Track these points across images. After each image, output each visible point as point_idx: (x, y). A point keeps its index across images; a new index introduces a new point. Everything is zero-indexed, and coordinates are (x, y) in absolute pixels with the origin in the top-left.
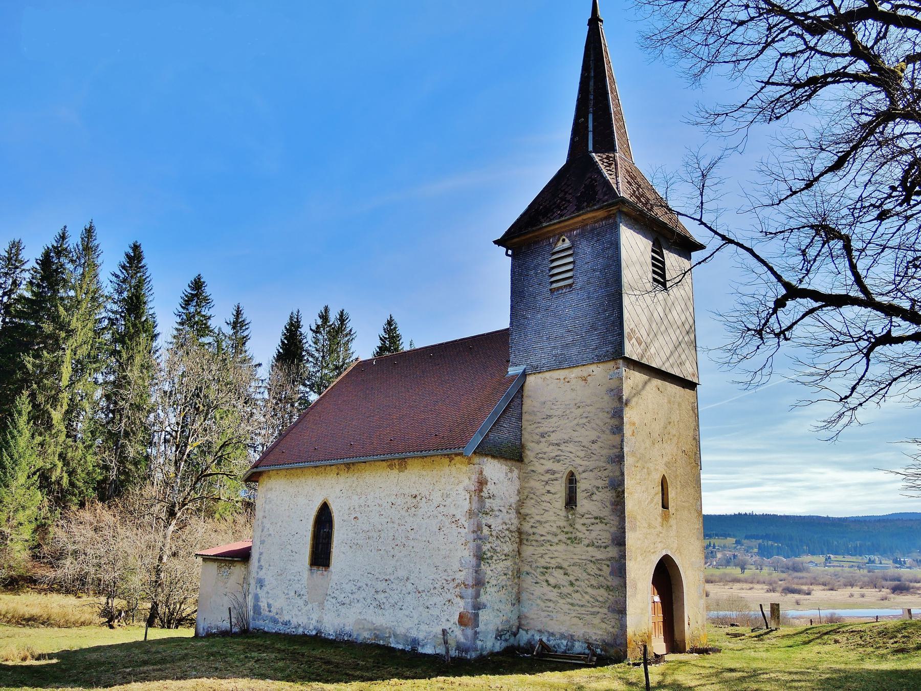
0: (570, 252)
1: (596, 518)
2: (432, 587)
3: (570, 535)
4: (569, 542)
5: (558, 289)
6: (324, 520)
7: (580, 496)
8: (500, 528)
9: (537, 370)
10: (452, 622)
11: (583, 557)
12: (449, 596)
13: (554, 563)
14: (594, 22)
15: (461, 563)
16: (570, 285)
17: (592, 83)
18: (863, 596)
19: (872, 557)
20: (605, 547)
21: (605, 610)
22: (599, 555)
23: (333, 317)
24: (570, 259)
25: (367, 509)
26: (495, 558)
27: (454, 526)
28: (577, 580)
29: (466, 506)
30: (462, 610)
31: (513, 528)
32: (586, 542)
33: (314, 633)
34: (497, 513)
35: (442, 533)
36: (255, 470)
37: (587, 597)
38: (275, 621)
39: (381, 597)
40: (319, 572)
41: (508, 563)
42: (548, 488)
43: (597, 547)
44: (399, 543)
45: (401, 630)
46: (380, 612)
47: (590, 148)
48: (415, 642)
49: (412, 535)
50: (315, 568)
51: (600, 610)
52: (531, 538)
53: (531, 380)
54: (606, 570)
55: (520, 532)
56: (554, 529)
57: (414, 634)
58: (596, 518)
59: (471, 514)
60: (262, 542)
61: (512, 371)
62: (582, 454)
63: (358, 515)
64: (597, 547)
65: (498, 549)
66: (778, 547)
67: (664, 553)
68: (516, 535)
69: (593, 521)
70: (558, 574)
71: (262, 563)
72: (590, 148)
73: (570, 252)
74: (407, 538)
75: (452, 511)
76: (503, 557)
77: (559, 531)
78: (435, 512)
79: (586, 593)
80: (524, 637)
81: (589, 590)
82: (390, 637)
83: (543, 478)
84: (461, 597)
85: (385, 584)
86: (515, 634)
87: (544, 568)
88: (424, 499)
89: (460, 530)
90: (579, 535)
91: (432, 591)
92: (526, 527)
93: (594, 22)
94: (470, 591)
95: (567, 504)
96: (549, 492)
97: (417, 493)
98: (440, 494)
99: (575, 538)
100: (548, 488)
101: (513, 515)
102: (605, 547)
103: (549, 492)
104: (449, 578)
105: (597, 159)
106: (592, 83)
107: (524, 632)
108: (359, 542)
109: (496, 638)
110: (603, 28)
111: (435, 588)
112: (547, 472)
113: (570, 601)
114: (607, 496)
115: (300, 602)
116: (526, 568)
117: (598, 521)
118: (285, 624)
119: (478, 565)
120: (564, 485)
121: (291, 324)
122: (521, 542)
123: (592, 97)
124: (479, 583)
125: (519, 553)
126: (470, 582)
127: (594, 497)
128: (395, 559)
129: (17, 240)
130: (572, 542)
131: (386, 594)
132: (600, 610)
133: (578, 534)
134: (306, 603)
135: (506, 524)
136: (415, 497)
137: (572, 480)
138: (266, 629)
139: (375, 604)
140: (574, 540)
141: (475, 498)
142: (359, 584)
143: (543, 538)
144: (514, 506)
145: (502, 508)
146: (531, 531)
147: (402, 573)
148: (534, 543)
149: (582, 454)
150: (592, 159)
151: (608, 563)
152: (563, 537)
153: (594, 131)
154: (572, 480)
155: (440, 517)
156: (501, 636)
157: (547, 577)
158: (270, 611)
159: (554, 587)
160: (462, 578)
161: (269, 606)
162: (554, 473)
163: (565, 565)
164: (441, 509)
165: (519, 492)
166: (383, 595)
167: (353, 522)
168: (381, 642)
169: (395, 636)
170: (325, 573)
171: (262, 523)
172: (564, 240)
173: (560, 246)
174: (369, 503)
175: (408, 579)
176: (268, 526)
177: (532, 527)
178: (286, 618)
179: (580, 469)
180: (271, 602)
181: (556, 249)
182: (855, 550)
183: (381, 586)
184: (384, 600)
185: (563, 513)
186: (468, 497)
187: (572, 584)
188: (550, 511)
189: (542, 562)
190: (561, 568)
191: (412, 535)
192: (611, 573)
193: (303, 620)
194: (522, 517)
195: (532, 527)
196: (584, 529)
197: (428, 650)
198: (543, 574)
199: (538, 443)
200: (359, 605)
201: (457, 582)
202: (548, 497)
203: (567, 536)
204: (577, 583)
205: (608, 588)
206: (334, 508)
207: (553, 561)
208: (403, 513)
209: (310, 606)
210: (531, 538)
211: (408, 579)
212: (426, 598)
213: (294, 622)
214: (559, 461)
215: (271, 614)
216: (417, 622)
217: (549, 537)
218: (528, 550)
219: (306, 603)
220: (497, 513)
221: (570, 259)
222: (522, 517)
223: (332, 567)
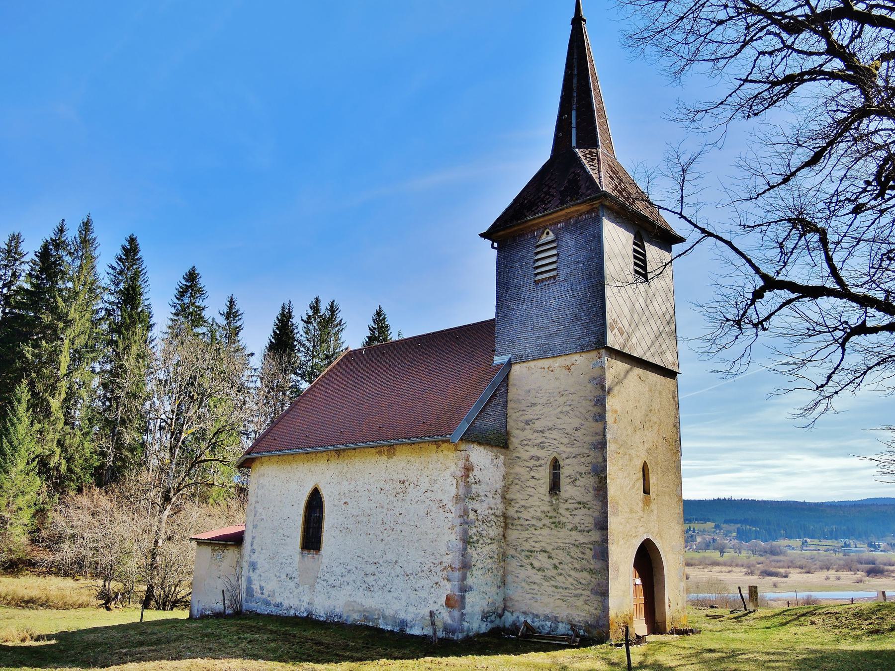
0: (554, 245)
1: (579, 503)
2: (420, 570)
3: (554, 520)
4: (553, 526)
6: (315, 505)
7: (564, 481)
8: (486, 513)
9: (522, 359)
10: (439, 604)
11: (567, 541)
12: (436, 579)
13: (538, 547)
14: (577, 21)
15: (448, 547)
16: (554, 277)
17: (575, 81)
18: (838, 579)
19: (848, 541)
20: (588, 532)
21: (588, 593)
22: (582, 539)
23: (324, 308)
24: (554, 252)
25: (357, 494)
26: (481, 541)
27: (441, 510)
28: (560, 563)
29: (453, 491)
30: (449, 592)
31: (499, 513)
32: (570, 526)
33: (305, 614)
34: (483, 498)
35: (429, 518)
36: (248, 456)
37: (571, 580)
38: (268, 603)
39: (370, 579)
40: (310, 556)
41: (494, 547)
42: (532, 474)
43: (580, 531)
44: (388, 527)
45: (389, 612)
46: (369, 594)
47: (574, 144)
48: (403, 623)
49: (400, 519)
51: (583, 592)
52: (516, 522)
54: (589, 554)
55: (505, 517)
56: (539, 514)
57: (402, 615)
58: (579, 503)
59: (458, 499)
60: (255, 526)
61: (498, 360)
62: (565, 441)
63: (348, 500)
64: (580, 531)
65: (484, 533)
66: (756, 532)
67: (645, 537)
68: (501, 519)
69: (576, 505)
70: (543, 557)
71: (255, 547)
72: (574, 144)
73: (554, 245)
75: (440, 496)
76: (489, 541)
77: (543, 516)
78: (423, 498)
79: (570, 576)
80: (509, 619)
81: (573, 573)
82: (379, 618)
84: (448, 580)
85: (374, 567)
86: (500, 616)
87: (528, 551)
89: (447, 515)
90: (563, 519)
91: (420, 574)
92: (511, 512)
93: (577, 21)
94: (457, 574)
95: (551, 490)
96: (533, 478)
97: (406, 479)
98: (427, 479)
99: (559, 523)
100: (532, 474)
101: (499, 500)
102: (588, 532)
103: (533, 478)
105: (580, 154)
106: (575, 81)
107: (509, 614)
109: (482, 619)
110: (586, 27)
111: (423, 571)
112: (532, 458)
113: (554, 583)
114: (590, 481)
115: (292, 585)
117: (581, 506)
118: (277, 606)
119: (465, 549)
121: (283, 315)
122: (506, 527)
123: (575, 95)
124: (466, 566)
125: (504, 537)
126: (457, 565)
127: (577, 483)
128: (384, 542)
130: (556, 526)
131: (375, 577)
132: (583, 592)
133: (562, 518)
134: (297, 586)
135: (492, 509)
136: (403, 483)
137: (555, 466)
138: (258, 611)
139: (364, 586)
140: (558, 525)
141: (462, 484)
142: (349, 567)
143: (527, 523)
144: (500, 491)
145: (488, 494)
146: (516, 516)
147: (390, 557)
148: (519, 527)
149: (565, 441)
150: (575, 154)
151: (591, 546)
152: (547, 521)
153: (577, 128)
154: (555, 466)
155: (428, 502)
156: (486, 618)
157: (532, 560)
158: (262, 594)
159: (539, 570)
160: (449, 561)
161: (262, 588)
162: (538, 459)
163: (549, 549)
164: (429, 494)
165: (504, 478)
166: (372, 578)
167: (343, 507)
169: (384, 617)
170: (316, 556)
172: (548, 233)
173: (545, 238)
174: (358, 488)
175: (396, 562)
176: (260, 510)
177: (517, 511)
179: (564, 456)
180: (263, 584)
181: (541, 242)
182: (831, 534)
183: (370, 569)
184: (374, 583)
185: (547, 498)
186: (454, 482)
187: (555, 567)
188: (534, 497)
189: (527, 546)
190: (545, 552)
191: (400, 519)
192: (594, 557)
193: (294, 602)
194: (507, 502)
195: (517, 511)
196: (567, 513)
197: (416, 631)
198: (528, 557)
199: (523, 430)
200: (349, 588)
201: (444, 565)
202: (532, 483)
203: (551, 520)
204: (561, 566)
205: (591, 571)
206: (325, 493)
207: (537, 545)
208: (392, 498)
209: (301, 588)
210: (516, 522)
211: (396, 562)
212: (414, 581)
213: (286, 603)
214: (543, 448)
215: (264, 596)
216: (405, 604)
217: (534, 522)
218: (513, 535)
219: (297, 586)
220: (483, 498)
221: (554, 252)
222: (507, 502)
223: (323, 551)
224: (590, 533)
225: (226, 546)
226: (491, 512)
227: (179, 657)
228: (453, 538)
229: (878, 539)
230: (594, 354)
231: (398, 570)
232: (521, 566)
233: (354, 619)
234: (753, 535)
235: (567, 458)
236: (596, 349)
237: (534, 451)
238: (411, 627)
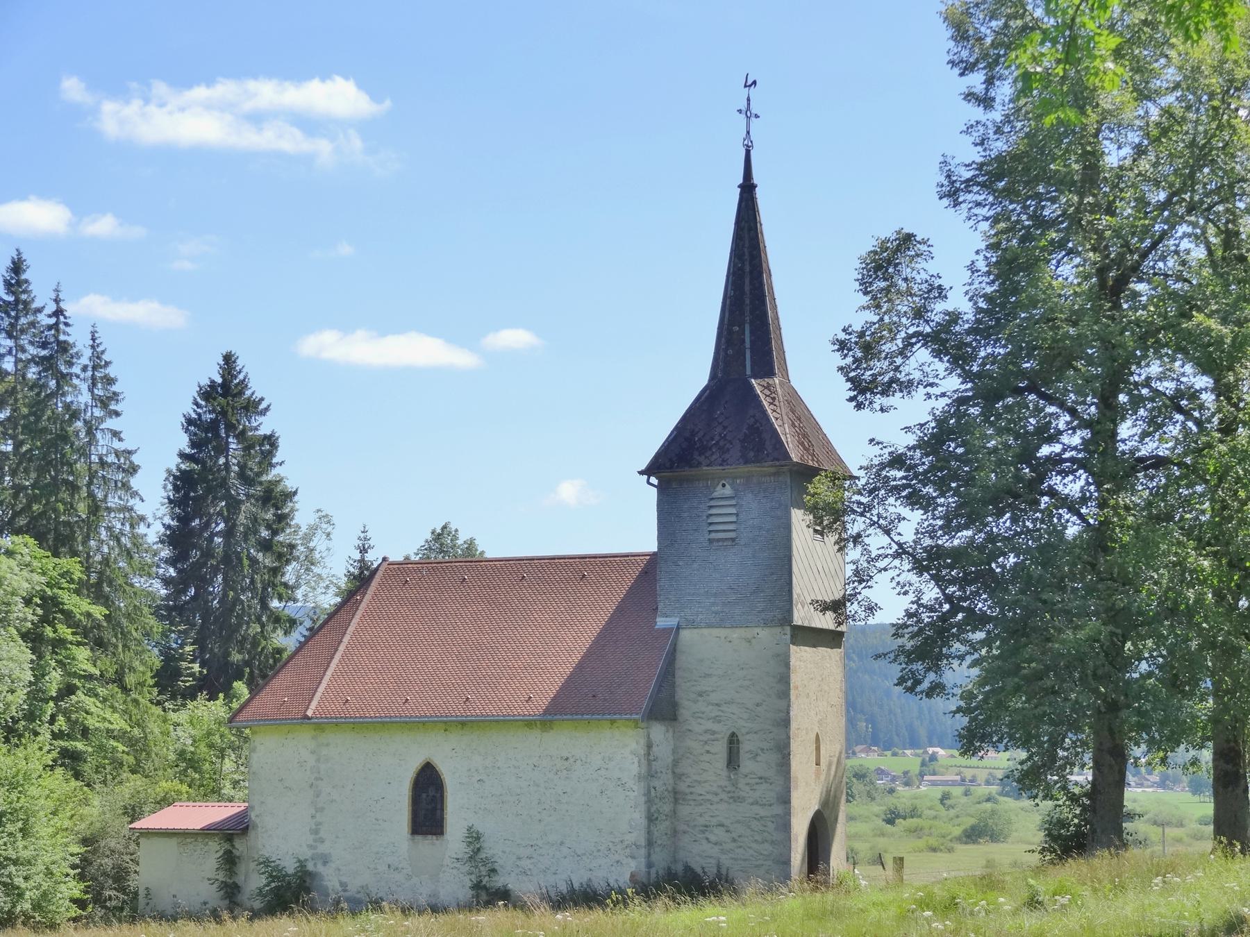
0: (733, 502)
5: (718, 540)
9: (692, 625)
12: (617, 857)
13: (714, 821)
14: (748, 189)
16: (733, 540)
17: (747, 281)
21: (769, 863)
22: (762, 812)
24: (733, 511)
27: (620, 789)
29: (635, 769)
32: (751, 800)
37: (751, 852)
39: (526, 863)
40: (426, 844)
41: (667, 823)
42: (707, 748)
46: (525, 878)
47: (748, 372)
52: (689, 797)
53: (685, 635)
54: (771, 826)
55: (675, 792)
56: (715, 789)
59: (640, 778)
61: (662, 622)
62: (745, 716)
63: (484, 777)
70: (720, 832)
72: (748, 372)
73: (733, 502)
77: (719, 791)
81: (754, 845)
83: (701, 738)
84: (633, 857)
92: (682, 787)
93: (748, 189)
94: (643, 851)
96: (708, 752)
100: (707, 748)
101: (670, 776)
103: (708, 752)
104: (617, 840)
105: (758, 390)
106: (747, 281)
110: (759, 193)
112: (706, 731)
114: (774, 757)
116: (683, 827)
119: (649, 827)
122: (676, 801)
123: (748, 301)
124: (650, 843)
126: (643, 842)
127: (759, 759)
137: (733, 742)
140: (737, 799)
141: (644, 762)
146: (688, 791)
149: (745, 716)
150: (752, 388)
152: (724, 796)
153: (752, 349)
154: (733, 742)
157: (707, 835)
158: (345, 891)
159: (716, 844)
162: (714, 733)
163: (727, 822)
164: (603, 772)
172: (724, 485)
173: (719, 491)
179: (744, 731)
180: (344, 879)
181: (716, 494)
185: (725, 773)
186: (636, 760)
187: (734, 840)
188: (709, 770)
189: (701, 821)
190: (723, 825)
194: (678, 776)
196: (747, 788)
198: (703, 832)
199: (695, 702)
202: (707, 757)
205: (773, 842)
210: (689, 797)
211: (562, 843)
214: (719, 722)
215: (347, 894)
217: (709, 797)
218: (684, 810)
219: (409, 877)
221: (733, 511)
222: (678, 776)
227: (836, 819)
228: (639, 817)
230: (778, 630)
236: (782, 625)
237: (710, 725)
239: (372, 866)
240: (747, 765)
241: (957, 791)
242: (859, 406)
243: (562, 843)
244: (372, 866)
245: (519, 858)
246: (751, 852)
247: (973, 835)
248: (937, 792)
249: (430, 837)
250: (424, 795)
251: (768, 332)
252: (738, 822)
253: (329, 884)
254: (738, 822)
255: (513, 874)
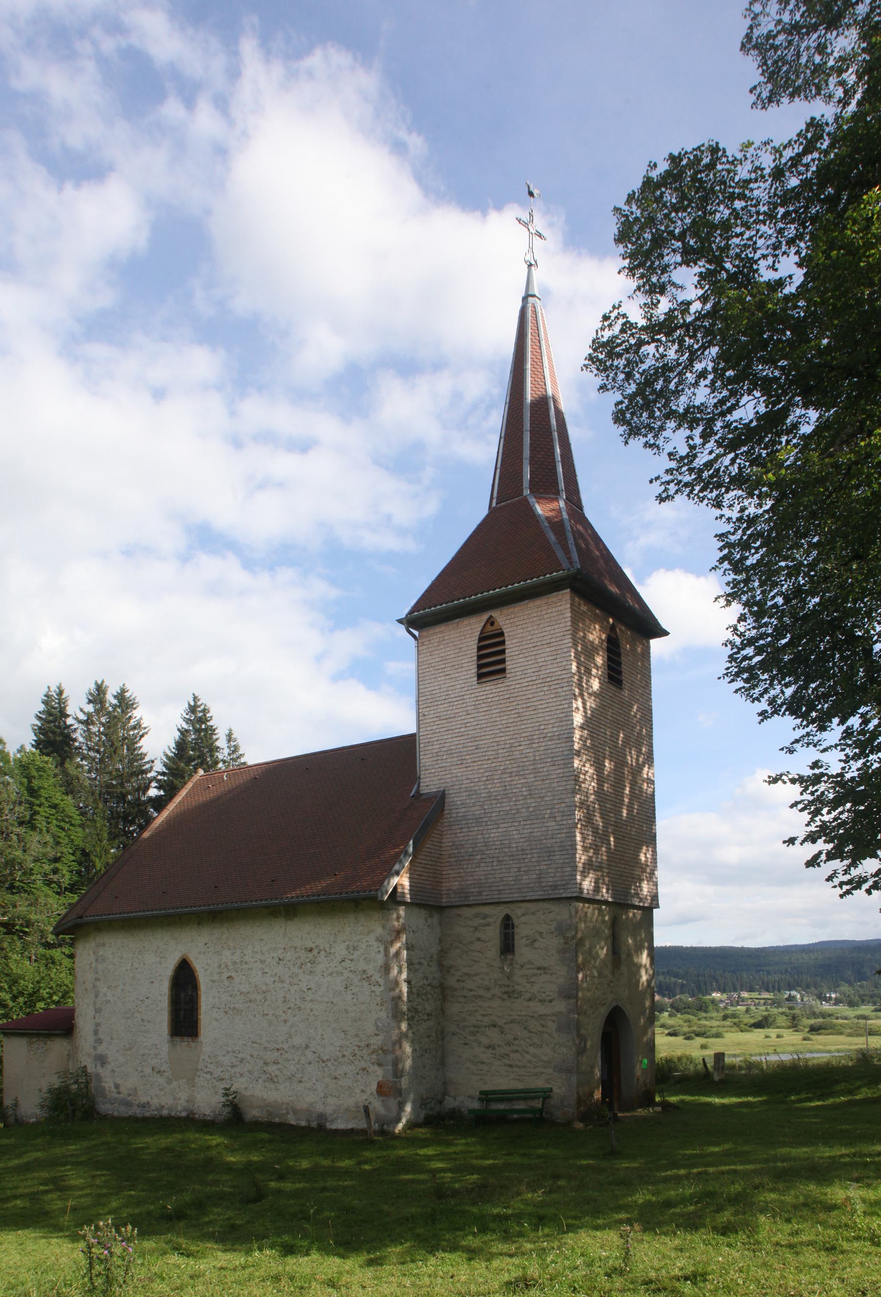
1: (539, 968)
2: (340, 1054)
3: (506, 989)
4: (505, 996)
6: (184, 981)
7: (520, 942)
8: (421, 983)
10: (369, 1092)
11: (523, 1013)
12: (363, 1064)
15: (377, 1027)
19: (793, 993)
20: (550, 1001)
21: (550, 1071)
22: (542, 1009)
25: (244, 966)
26: (417, 1018)
27: (365, 983)
28: (515, 1039)
30: (380, 1079)
31: (435, 983)
32: (528, 995)
33: (184, 1114)
34: (417, 967)
35: (349, 992)
36: (79, 921)
38: (128, 1104)
39: (272, 1069)
40: (184, 1045)
41: (432, 1023)
42: (478, 935)
43: (540, 1001)
44: (292, 1005)
45: (302, 1105)
48: (322, 1116)
49: (309, 996)
50: (178, 1039)
51: (544, 1070)
55: (443, 987)
57: (319, 1108)
58: (539, 968)
60: (98, 1011)
63: (233, 974)
64: (540, 1001)
65: (420, 1008)
66: (682, 985)
67: (614, 1004)
68: (438, 991)
69: (535, 971)
71: (101, 1035)
74: (303, 999)
75: (362, 966)
76: (426, 1017)
78: (340, 968)
79: (527, 1052)
80: (450, 1103)
82: (288, 1113)
84: (380, 1065)
85: (276, 1054)
86: (441, 1102)
87: (475, 1026)
88: (323, 953)
89: (373, 988)
90: (518, 988)
91: (341, 1060)
92: (451, 981)
96: (479, 939)
97: (314, 945)
98: (343, 946)
99: (513, 992)
100: (478, 935)
101: (434, 968)
102: (550, 1001)
103: (479, 939)
104: (362, 1044)
107: (451, 1099)
108: (237, 1006)
109: (421, 1107)
111: (344, 1056)
113: (507, 1062)
115: (161, 1080)
117: (541, 972)
118: (143, 1106)
120: (498, 931)
125: (443, 1012)
127: (537, 945)
128: (289, 1024)
129: (54, 688)
130: (510, 997)
131: (279, 1066)
132: (544, 1070)
133: (516, 987)
134: (169, 1081)
135: (427, 979)
136: (311, 950)
138: (115, 1114)
139: (264, 1077)
142: (241, 1055)
143: (474, 993)
144: (435, 957)
145: (423, 961)
147: (297, 1041)
148: (461, 1000)
149: (77, 812)
151: (554, 1018)
152: (497, 991)
155: (346, 974)
156: (426, 1105)
158: (119, 1093)
160: (379, 1043)
161: (117, 1086)
164: (347, 964)
165: (441, 941)
166: (275, 1067)
167: (226, 983)
168: (277, 1120)
170: (193, 1044)
171: (94, 986)
174: (247, 958)
176: (104, 990)
177: (458, 981)
178: (144, 1100)
182: (773, 987)
183: (271, 1056)
184: (277, 1073)
190: (494, 1026)
191: (309, 996)
192: (559, 1029)
195: (458, 981)
200: (244, 1080)
201: (373, 1047)
203: (503, 990)
204: (516, 1042)
206: (198, 965)
207: (486, 1019)
209: (175, 1083)
211: (307, 1047)
212: (333, 1068)
213: (155, 1102)
215: (121, 1096)
216: (322, 1095)
217: (481, 992)
219: (169, 1081)
220: (417, 967)
224: (554, 1003)
225: (49, 1036)
226: (426, 982)
229: (830, 991)
231: (310, 1056)
232: (466, 1044)
233: (254, 1116)
234: (678, 990)
235: (523, 915)
238: (332, 1121)
239: (140, 1069)
240: (523, 953)
241: (753, 1008)
242: (634, 431)
243: (307, 1047)
244: (140, 1069)
245: (266, 1063)
246: (528, 1057)
247: (758, 1025)
248: (744, 1008)
249: (186, 1039)
250: (183, 995)
251: (510, 403)
252: (513, 1021)
253: (106, 1086)
254: (513, 1021)
255: (260, 1081)
